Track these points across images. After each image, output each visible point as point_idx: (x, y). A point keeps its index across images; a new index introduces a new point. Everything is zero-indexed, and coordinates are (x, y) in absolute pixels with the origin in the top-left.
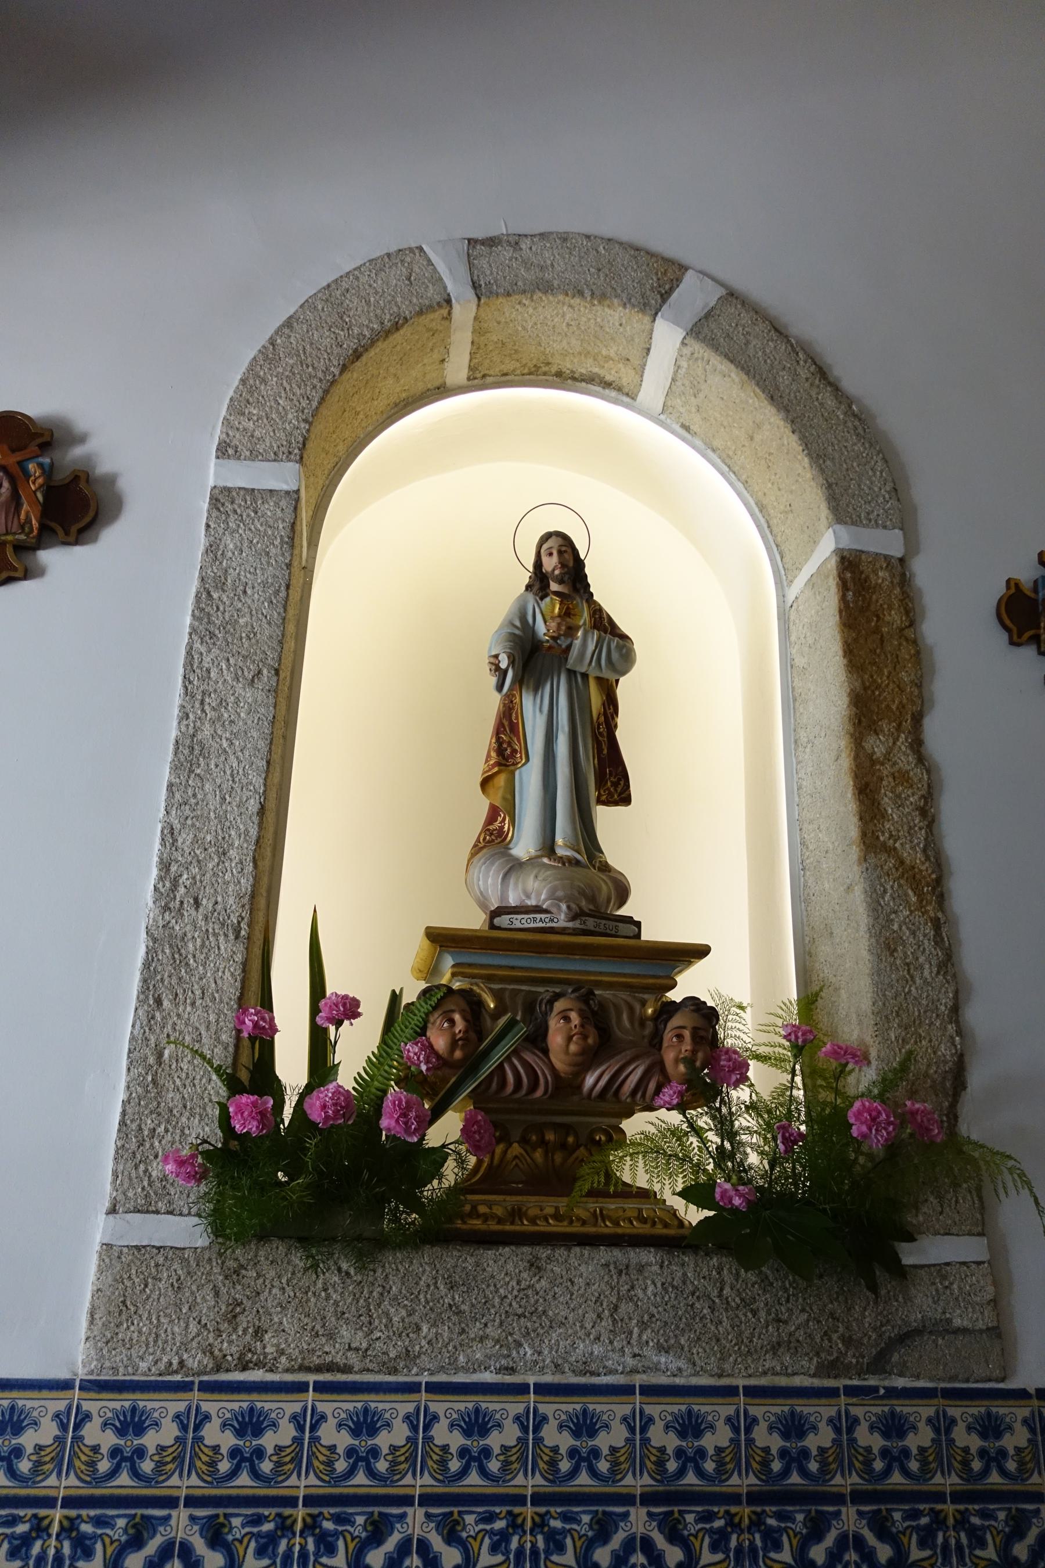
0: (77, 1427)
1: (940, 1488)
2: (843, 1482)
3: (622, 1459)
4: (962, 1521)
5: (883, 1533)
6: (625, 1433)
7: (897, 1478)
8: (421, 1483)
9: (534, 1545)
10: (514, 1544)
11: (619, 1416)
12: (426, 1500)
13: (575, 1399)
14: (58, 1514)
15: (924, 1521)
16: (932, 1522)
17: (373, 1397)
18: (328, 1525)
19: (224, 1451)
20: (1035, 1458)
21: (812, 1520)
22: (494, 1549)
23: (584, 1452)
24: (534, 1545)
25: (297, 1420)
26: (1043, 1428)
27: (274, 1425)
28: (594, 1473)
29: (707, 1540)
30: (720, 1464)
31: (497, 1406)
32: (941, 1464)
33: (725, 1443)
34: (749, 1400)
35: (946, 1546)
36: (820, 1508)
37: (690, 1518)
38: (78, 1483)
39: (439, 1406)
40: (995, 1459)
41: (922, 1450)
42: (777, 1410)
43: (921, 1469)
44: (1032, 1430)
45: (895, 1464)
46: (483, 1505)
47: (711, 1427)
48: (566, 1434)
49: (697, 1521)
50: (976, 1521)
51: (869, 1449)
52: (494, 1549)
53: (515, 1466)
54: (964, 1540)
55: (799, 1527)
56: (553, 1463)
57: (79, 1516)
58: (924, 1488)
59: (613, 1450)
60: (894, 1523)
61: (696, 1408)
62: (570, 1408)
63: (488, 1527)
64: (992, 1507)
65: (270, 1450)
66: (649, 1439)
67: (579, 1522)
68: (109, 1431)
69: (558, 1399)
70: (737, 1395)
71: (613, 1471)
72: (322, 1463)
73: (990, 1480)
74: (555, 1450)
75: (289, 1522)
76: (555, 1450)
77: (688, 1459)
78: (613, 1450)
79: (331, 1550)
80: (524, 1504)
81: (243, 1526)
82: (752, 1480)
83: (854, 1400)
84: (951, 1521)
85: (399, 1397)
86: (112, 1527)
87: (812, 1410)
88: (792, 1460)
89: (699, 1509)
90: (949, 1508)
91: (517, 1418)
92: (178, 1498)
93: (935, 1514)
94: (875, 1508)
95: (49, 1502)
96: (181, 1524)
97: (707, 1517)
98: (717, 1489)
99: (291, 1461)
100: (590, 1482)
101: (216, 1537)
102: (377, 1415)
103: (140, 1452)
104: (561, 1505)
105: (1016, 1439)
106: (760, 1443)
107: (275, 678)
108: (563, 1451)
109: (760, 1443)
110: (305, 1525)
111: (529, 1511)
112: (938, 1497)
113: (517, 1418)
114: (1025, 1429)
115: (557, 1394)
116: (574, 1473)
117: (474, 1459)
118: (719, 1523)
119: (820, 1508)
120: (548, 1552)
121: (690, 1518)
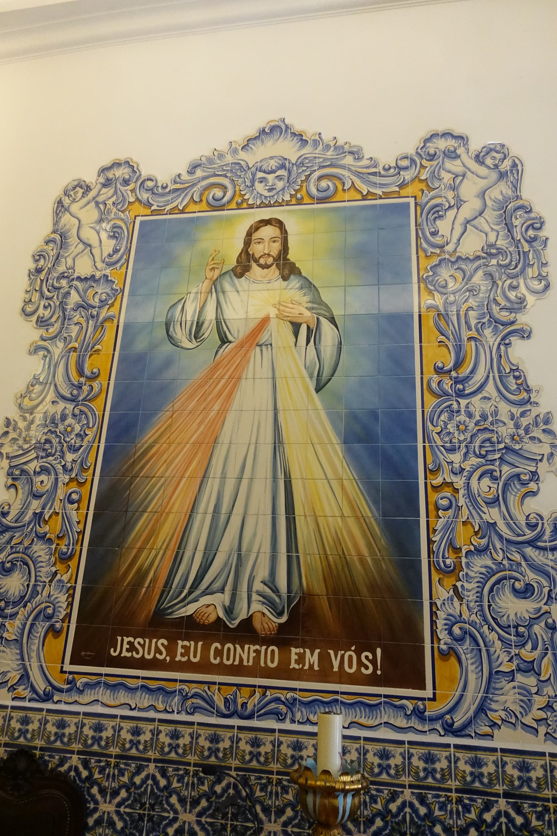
2: (151, 754)
4: (279, 782)
5: (519, 811)
7: (254, 763)
8: (76, 747)
10: (107, 772)
11: (269, 740)
12: (156, 761)
13: (379, 744)
14: (191, 769)
16: (543, 810)
17: (301, 737)
18: (122, 766)
19: (90, 737)
21: (485, 803)
22: (178, 781)
23: (135, 741)
25: (273, 743)
27: (69, 726)
28: (177, 753)
29: (97, 770)
32: (232, 755)
33: (110, 735)
34: (456, 750)
35: (271, 793)
36: (489, 798)
37: (170, 769)
39: (284, 739)
40: (385, 769)
41: (185, 745)
42: (250, 736)
43: (183, 753)
45: (213, 754)
47: (486, 764)
48: (248, 745)
49: (173, 771)
51: (418, 767)
52: (178, 781)
53: (544, 786)
54: (196, 781)
58: (68, 748)
59: (146, 741)
61: (258, 736)
63: (534, 810)
70: (497, 752)
71: (32, 738)
74: (87, 736)
75: (450, 799)
76: (87, 736)
77: (96, 740)
78: (146, 741)
80: (231, 770)
81: (255, 780)
85: (228, 730)
86: (54, 758)
88: (59, 737)
89: (434, 793)
90: (113, 760)
91: (151, 731)
93: (269, 779)
100: (432, 781)
102: (141, 729)
108: (90, 737)
109: (123, 737)
110: (115, 766)
111: (454, 795)
113: (151, 731)
114: (446, 761)
116: (169, 752)
119: (489, 798)
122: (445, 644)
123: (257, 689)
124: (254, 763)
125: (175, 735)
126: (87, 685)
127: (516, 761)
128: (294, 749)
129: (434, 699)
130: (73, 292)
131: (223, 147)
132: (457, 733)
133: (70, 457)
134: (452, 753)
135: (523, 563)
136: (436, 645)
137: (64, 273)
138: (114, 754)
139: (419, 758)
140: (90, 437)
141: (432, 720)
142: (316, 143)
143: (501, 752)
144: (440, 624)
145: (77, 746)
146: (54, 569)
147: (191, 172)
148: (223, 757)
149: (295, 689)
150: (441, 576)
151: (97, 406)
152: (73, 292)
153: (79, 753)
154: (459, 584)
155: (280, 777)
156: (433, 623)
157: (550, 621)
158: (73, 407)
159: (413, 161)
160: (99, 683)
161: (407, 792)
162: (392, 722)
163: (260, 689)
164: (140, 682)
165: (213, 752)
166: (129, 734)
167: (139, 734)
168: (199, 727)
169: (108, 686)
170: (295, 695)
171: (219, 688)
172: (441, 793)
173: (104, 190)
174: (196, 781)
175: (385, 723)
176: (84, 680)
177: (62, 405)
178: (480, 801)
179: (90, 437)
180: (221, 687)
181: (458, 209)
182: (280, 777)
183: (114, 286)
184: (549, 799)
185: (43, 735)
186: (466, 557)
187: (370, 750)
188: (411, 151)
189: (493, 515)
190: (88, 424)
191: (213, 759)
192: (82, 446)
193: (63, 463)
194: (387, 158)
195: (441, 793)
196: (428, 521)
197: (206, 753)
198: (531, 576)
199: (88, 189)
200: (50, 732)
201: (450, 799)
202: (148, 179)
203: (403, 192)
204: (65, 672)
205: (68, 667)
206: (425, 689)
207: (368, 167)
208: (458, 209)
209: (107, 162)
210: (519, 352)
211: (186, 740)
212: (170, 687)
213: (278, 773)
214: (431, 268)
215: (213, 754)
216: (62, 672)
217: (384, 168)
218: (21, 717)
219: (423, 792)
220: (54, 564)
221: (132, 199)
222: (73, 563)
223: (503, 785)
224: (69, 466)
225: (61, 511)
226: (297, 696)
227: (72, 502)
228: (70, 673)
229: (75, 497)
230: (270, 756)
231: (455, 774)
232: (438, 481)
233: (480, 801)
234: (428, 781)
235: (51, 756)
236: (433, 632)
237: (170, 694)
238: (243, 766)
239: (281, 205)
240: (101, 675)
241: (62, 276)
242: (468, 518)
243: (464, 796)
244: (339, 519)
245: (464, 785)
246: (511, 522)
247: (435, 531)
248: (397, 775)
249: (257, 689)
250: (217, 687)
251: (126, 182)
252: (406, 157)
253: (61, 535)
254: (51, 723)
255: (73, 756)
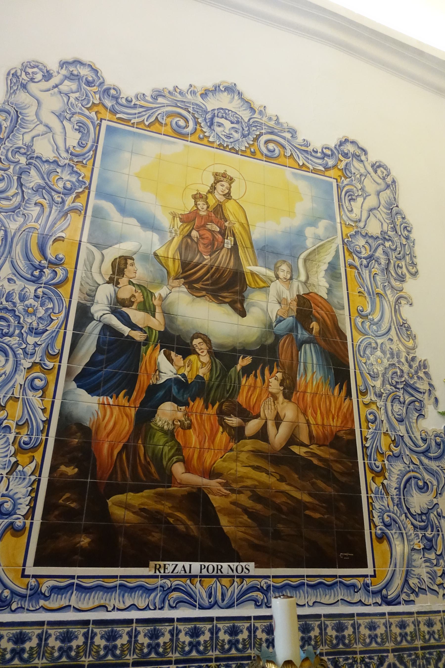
0: (390, 627)
1: (170, 659)
3: (125, 649)
6: (385, 629)
8: (390, 645)
9: (423, 663)
11: (382, 623)
14: (358, 656)
15: (350, 661)
17: (431, 615)
18: (367, 660)
20: (443, 633)
24: (423, 663)
25: (385, 624)
26: (444, 622)
30: (244, 645)
31: (202, 626)
32: (251, 645)
34: (94, 626)
36: (242, 662)
38: (47, 662)
39: (181, 627)
44: (442, 624)
45: (153, 650)
46: (182, 664)
50: (367, 660)
55: (375, 662)
56: (223, 646)
57: (220, 664)
60: (404, 658)
62: (190, 626)
64: (432, 651)
65: (75, 647)
66: (138, 640)
67: (374, 659)
68: (188, 637)
69: (9, 628)
70: (251, 620)
71: (439, 638)
72: (95, 652)
73: (192, 654)
76: (223, 641)
77: (64, 651)
79: (430, 664)
82: (135, 656)
83: (49, 628)
84: (359, 661)
85: (436, 614)
87: (202, 626)
92: (129, 664)
94: (334, 657)
95: (355, 653)
96: (391, 658)
97: (410, 655)
98: (204, 657)
99: (170, 647)
101: (402, 662)
103: (23, 650)
104: (225, 662)
105: (437, 627)
106: (182, 640)
107: (388, 437)
109: (182, 640)
110: (361, 661)
111: (420, 652)
112: (416, 649)
114: (209, 633)
115: (243, 620)
117: (110, 650)
118: (350, 661)
119: (242, 662)
120: (427, 665)
121: (341, 660)
122: (380, 529)
123: (236, 579)
124: (374, 645)
125: (403, 625)
126: (53, 589)
127: (334, 623)
128: (370, 629)
129: (374, 576)
130: (33, 172)
131: (184, 87)
132: (389, 603)
133: (31, 340)
134: (90, 629)
135: (421, 467)
136: (373, 531)
137: (20, 148)
138: (390, 648)
139: (186, 634)
140: (54, 325)
141: (374, 593)
142: (261, 113)
143: (216, 620)
144: (376, 514)
145: (132, 657)
146: (13, 460)
147: (155, 98)
148: (411, 640)
149: (268, 577)
150: (373, 475)
151: (64, 291)
152: (33, 172)
153: (394, 651)
154: (385, 482)
155: (363, 656)
156: (370, 513)
157: (439, 510)
158: (34, 288)
159: (333, 154)
160: (336, 583)
161: (391, 655)
162: (345, 599)
163: (238, 579)
164: (119, 582)
165: (153, 648)
166: (426, 626)
167: (237, 634)
168: (358, 618)
169: (80, 588)
170: (268, 582)
171: (200, 581)
172: (349, 656)
173: (66, 82)
174: (425, 663)
175: (341, 599)
176: (52, 583)
177: (20, 284)
178: (376, 658)
179: (54, 325)
180: (203, 579)
181: (364, 199)
182: (363, 656)
183: (80, 178)
184: (129, 664)
185: (420, 635)
186: (388, 461)
187: (221, 628)
188: (332, 146)
189: (402, 429)
190: (53, 309)
191: (110, 657)
192: (47, 330)
193: (24, 346)
194: (317, 144)
195: (349, 656)
196: (361, 431)
197: (368, 641)
198: (427, 477)
199: (48, 76)
200: (142, 644)
201: (356, 659)
202: (114, 89)
203: (327, 173)
204: (28, 576)
205: (31, 570)
206: (367, 567)
207: (301, 146)
208: (364, 199)
209: (69, 57)
210: (406, 311)
211: (207, 636)
212: (151, 583)
213: (361, 652)
214: (350, 236)
215: (110, 652)
216: (24, 576)
217: (313, 150)
218: (399, 622)
219: (187, 665)
220: (15, 455)
221: (97, 102)
222: (38, 455)
223: (133, 655)
224: (30, 349)
225: (21, 397)
226: (272, 583)
227: (34, 388)
228: (34, 576)
229: (38, 383)
230: (319, 639)
231: (390, 636)
232: (367, 399)
233: (376, 658)
234: (340, 647)
235: (370, 658)
236: (371, 520)
237: (148, 591)
238: (365, 649)
239: (237, 153)
240: (303, 576)
241: (17, 151)
242: (387, 431)
243: (365, 655)
244: (321, 427)
245: (97, 660)
246: (412, 435)
247: (366, 439)
248: (383, 642)
249: (236, 579)
250: (199, 579)
251: (89, 83)
252: (328, 148)
253: (21, 423)
254: (222, 631)
255: (389, 654)
